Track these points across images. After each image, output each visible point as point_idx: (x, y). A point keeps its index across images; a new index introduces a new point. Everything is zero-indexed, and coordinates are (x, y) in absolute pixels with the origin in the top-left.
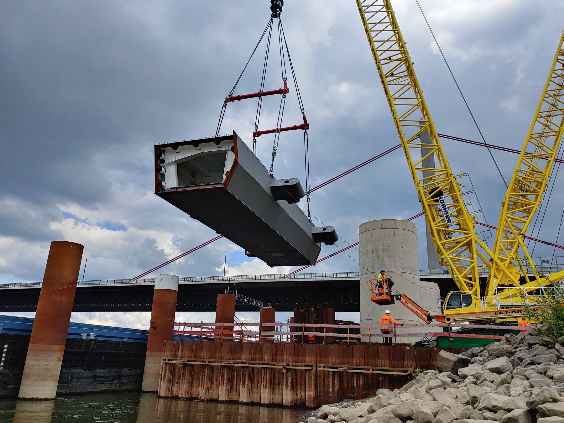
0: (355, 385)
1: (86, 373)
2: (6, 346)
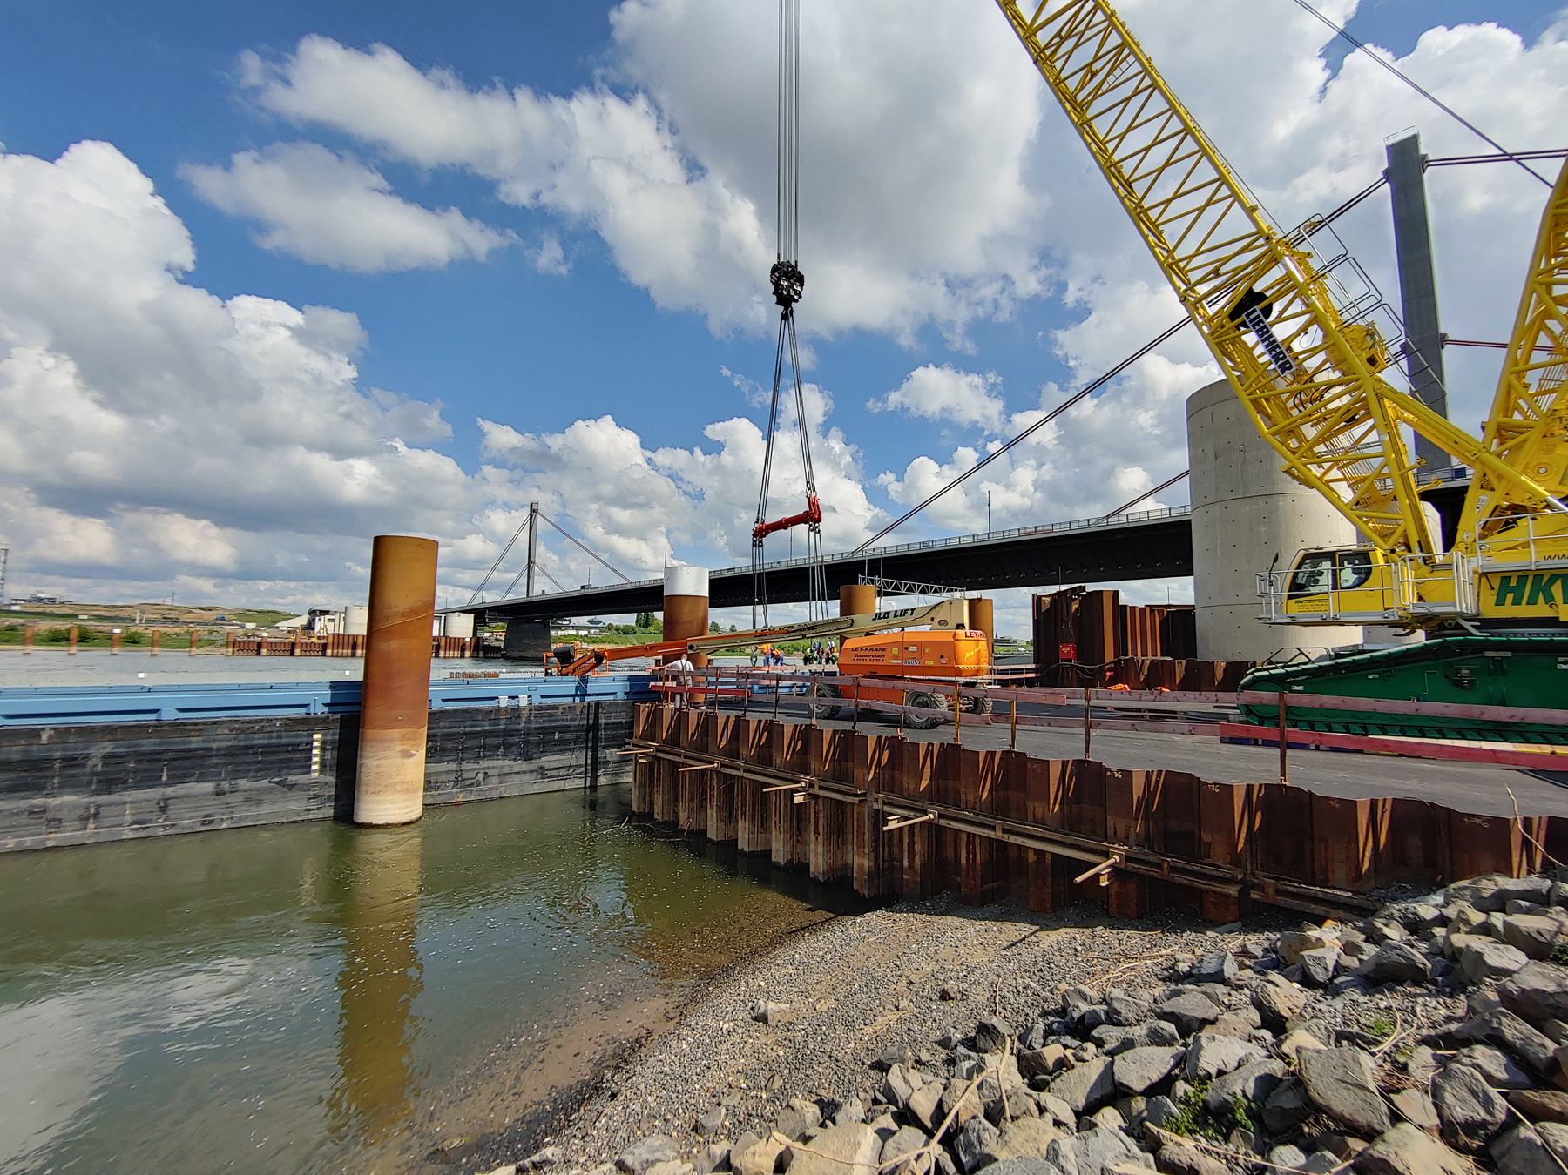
0: (963, 861)
1: (521, 765)
2: (316, 736)
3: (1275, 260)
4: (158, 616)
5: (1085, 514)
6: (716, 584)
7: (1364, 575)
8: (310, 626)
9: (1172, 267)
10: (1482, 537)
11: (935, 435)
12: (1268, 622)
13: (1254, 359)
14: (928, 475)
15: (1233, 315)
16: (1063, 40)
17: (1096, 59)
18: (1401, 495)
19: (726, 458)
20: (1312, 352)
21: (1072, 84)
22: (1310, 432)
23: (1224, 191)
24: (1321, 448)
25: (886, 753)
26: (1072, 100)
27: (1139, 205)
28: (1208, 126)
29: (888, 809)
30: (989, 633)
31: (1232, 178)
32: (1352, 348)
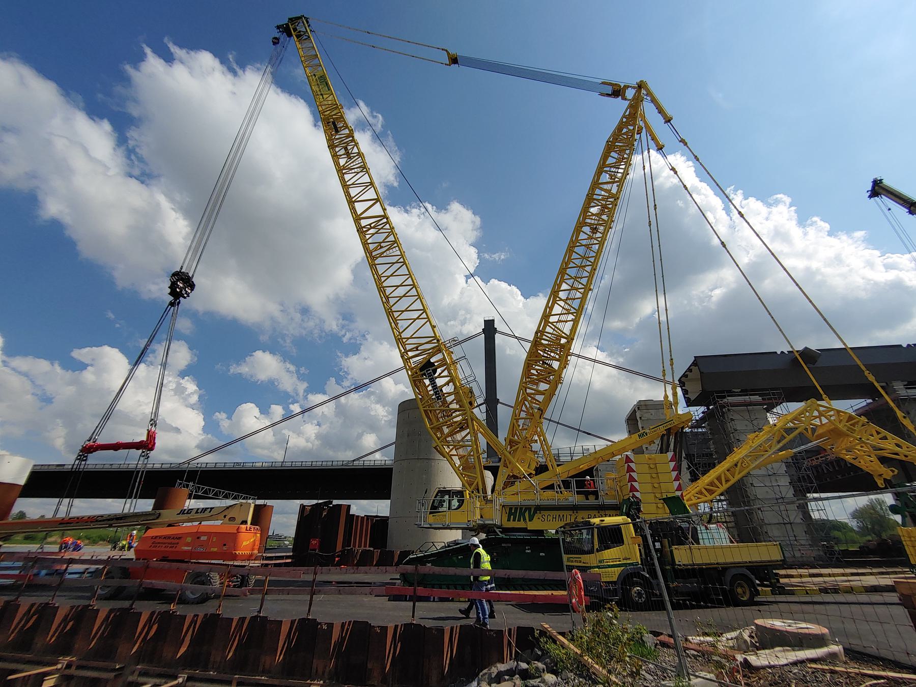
3: (440, 351)
5: (343, 456)
7: (461, 502)
9: (400, 341)
10: (503, 489)
11: (264, 394)
12: (419, 526)
13: (428, 392)
14: (250, 417)
15: (421, 369)
16: (371, 228)
17: (383, 242)
18: (477, 466)
19: (88, 376)
20: (450, 394)
21: (371, 247)
22: (446, 430)
23: (424, 316)
24: (449, 439)
25: (155, 627)
26: (371, 253)
27: (390, 308)
28: (421, 283)
29: (142, 679)
30: (264, 531)
31: (428, 311)
32: (465, 395)
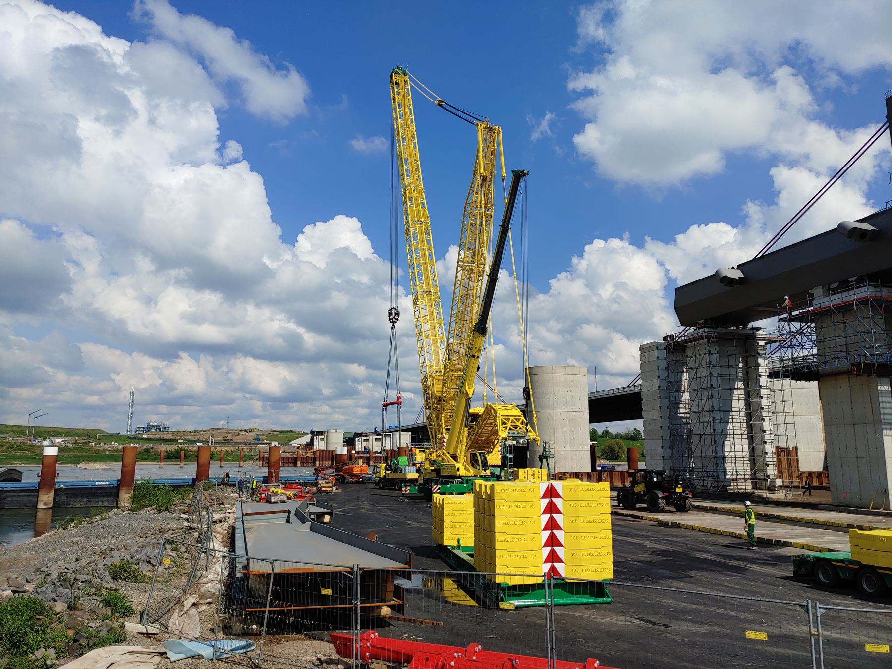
4: (220, 438)
6: (303, 523)
8: (310, 444)
